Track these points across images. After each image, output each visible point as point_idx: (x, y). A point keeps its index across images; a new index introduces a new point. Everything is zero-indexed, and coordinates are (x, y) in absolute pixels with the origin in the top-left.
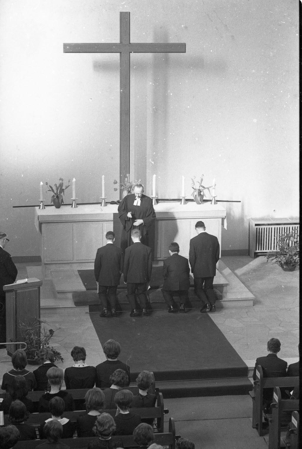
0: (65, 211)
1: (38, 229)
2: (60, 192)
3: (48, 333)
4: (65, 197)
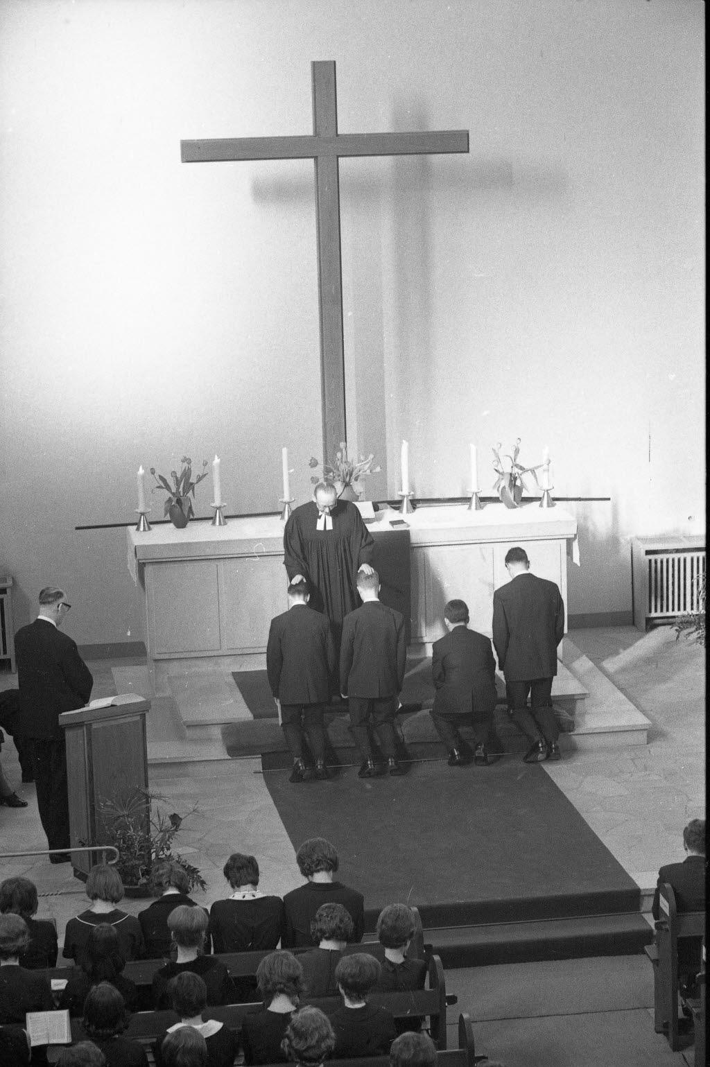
0: (198, 533)
1: (135, 577)
2: (186, 491)
3: (168, 823)
4: (197, 503)
